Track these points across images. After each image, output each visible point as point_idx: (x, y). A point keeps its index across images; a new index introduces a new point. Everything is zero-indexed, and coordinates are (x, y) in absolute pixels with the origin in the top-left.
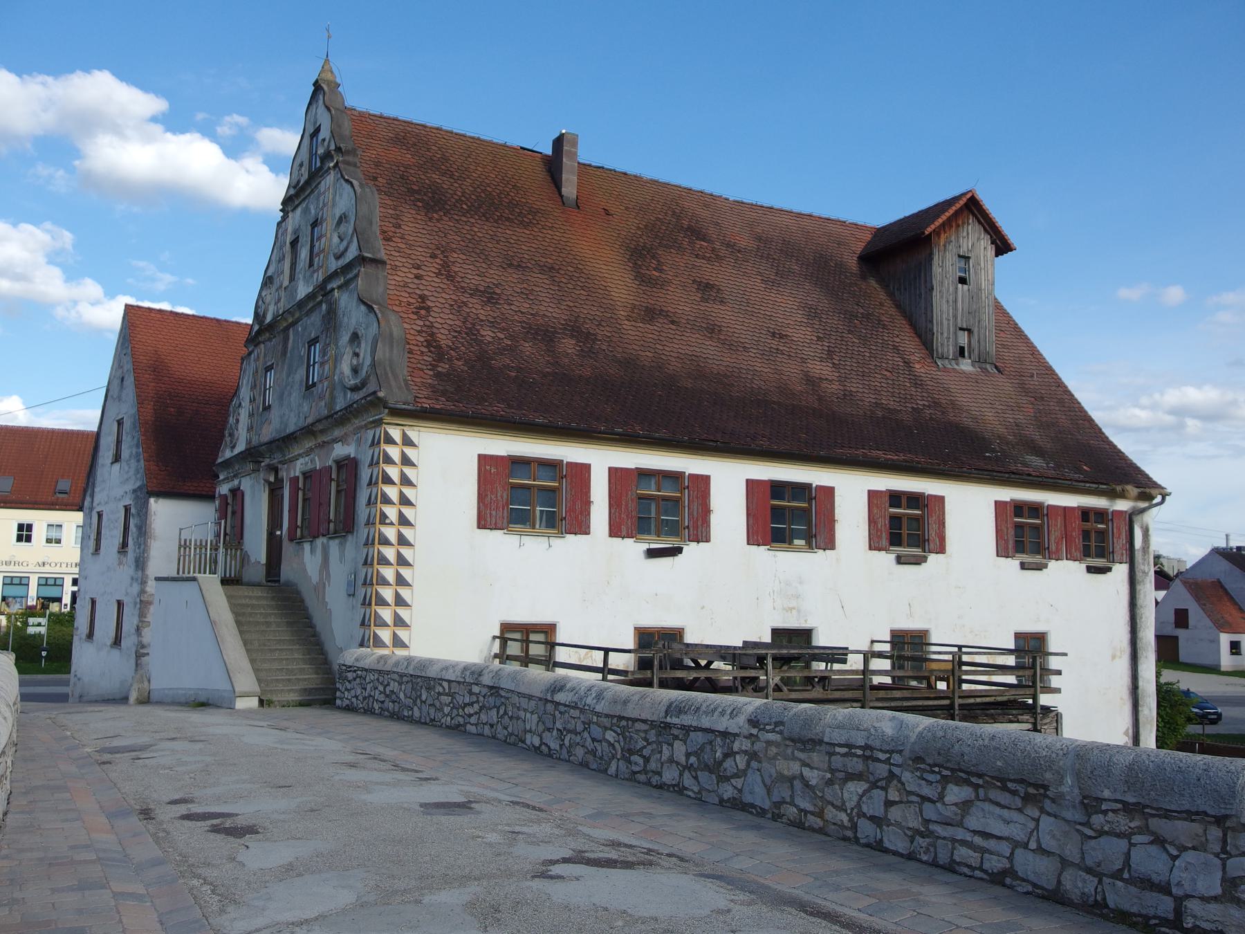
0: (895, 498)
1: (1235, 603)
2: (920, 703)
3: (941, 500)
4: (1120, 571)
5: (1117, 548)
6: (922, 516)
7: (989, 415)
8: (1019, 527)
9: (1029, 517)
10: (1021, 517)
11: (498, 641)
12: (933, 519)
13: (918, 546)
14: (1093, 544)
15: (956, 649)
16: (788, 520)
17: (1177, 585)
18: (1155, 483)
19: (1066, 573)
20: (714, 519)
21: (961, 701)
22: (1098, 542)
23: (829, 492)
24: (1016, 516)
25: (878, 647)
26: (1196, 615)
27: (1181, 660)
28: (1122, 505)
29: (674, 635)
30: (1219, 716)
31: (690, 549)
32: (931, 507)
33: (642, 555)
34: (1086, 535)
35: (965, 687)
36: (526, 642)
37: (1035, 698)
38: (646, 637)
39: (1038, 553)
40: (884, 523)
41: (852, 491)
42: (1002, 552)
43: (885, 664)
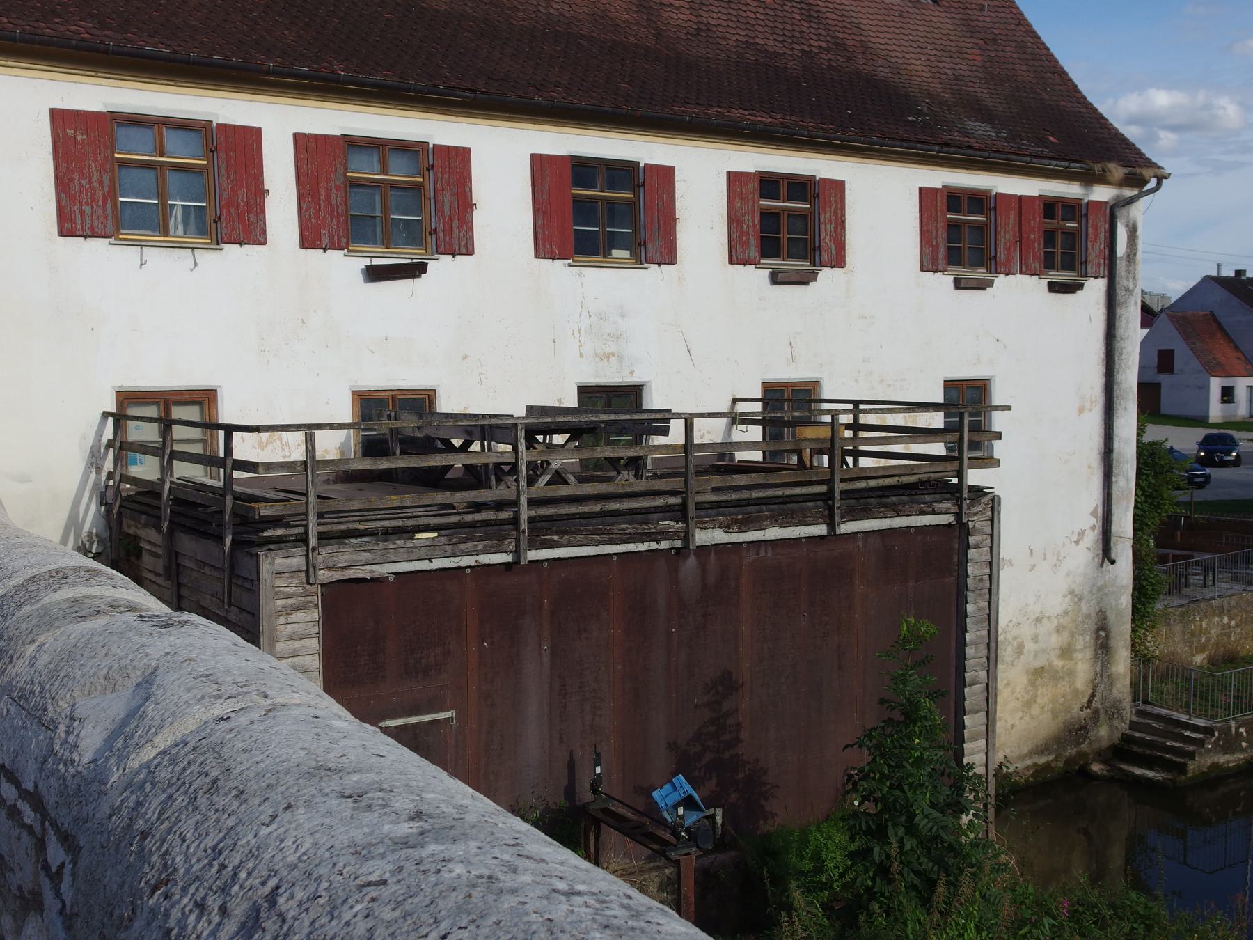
0: (769, 183)
1: (1230, 339)
2: (779, 492)
3: (838, 187)
4: (1095, 288)
5: (1092, 255)
6: (811, 212)
7: (917, 64)
8: (954, 227)
9: (970, 213)
10: (958, 211)
11: (111, 420)
12: (826, 217)
13: (804, 258)
14: (1059, 250)
15: (850, 406)
16: (600, 219)
17: (1163, 321)
18: (1149, 161)
19: (1019, 294)
20: (480, 218)
21: (844, 486)
22: (1067, 248)
23: (667, 174)
24: (950, 210)
25: (742, 407)
26: (1183, 356)
27: (1211, 421)
28: (1102, 194)
29: (421, 402)
30: (1207, 478)
31: (441, 267)
32: (823, 198)
33: (360, 277)
34: (1049, 237)
35: (864, 462)
36: (166, 424)
37: (960, 474)
38: (370, 404)
39: (981, 265)
40: (751, 223)
41: (702, 173)
42: (929, 264)
43: (755, 433)
